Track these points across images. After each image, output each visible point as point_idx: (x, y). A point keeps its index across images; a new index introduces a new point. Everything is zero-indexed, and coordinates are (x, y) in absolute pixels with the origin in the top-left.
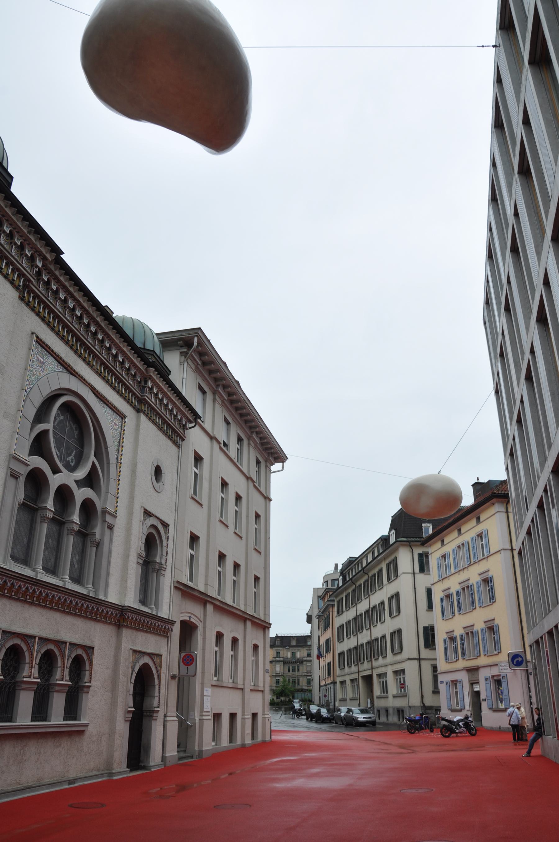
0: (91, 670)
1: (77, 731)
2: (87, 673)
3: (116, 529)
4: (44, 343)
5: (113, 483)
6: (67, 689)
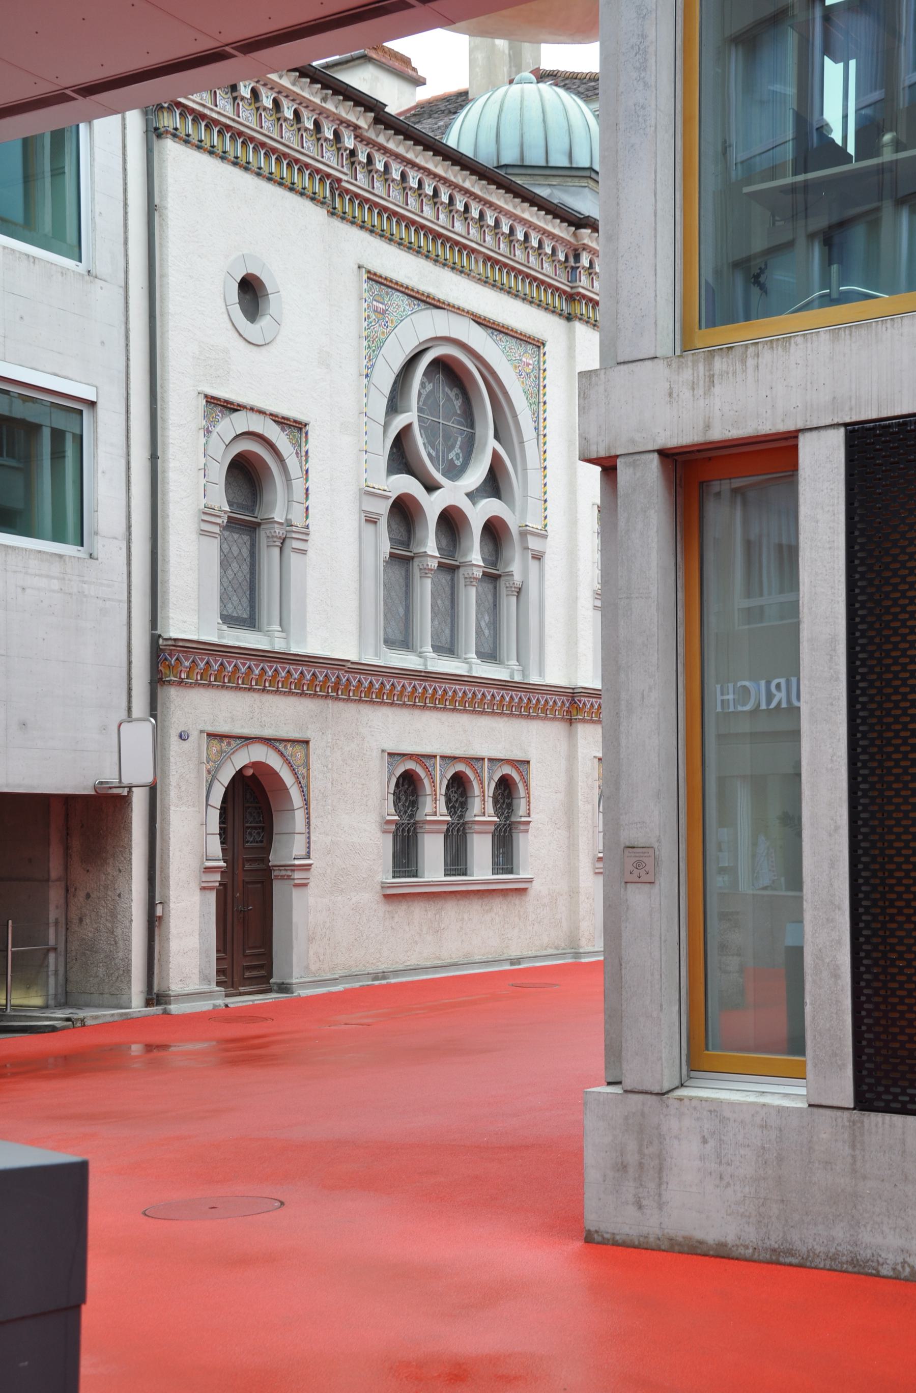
0: (529, 797)
1: (516, 889)
2: (523, 802)
3: (548, 560)
5: (534, 476)
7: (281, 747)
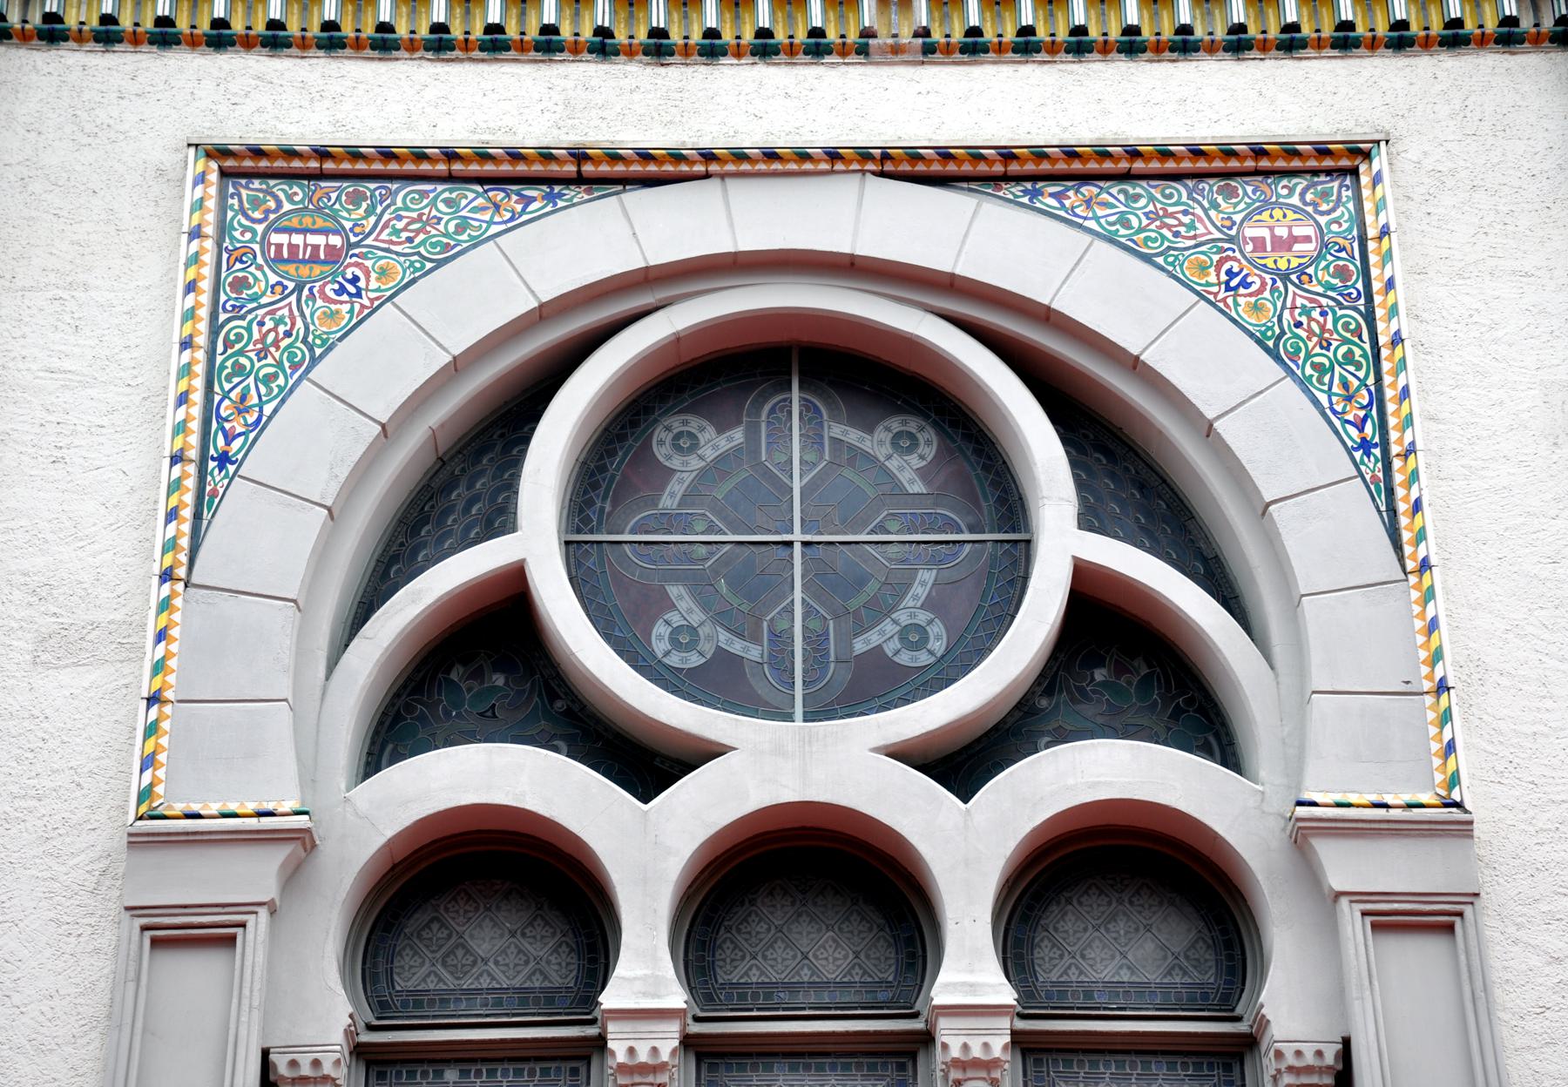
4: (354, 154)
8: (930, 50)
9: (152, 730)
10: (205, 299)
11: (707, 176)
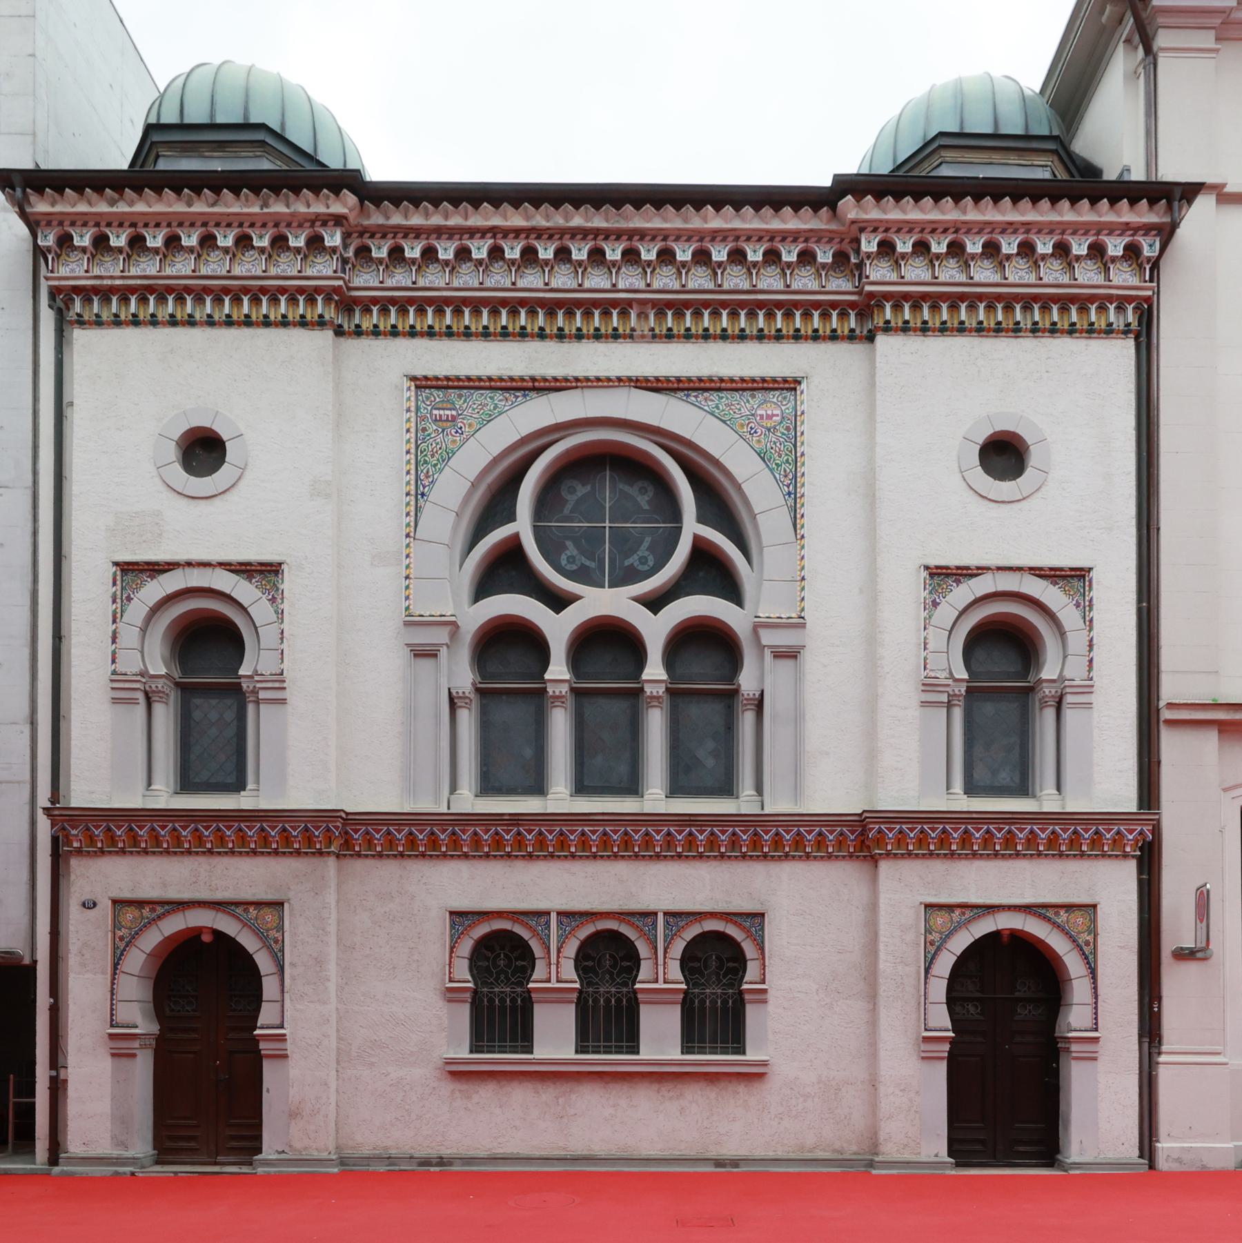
0: (764, 958)
4: (458, 379)
6: (575, 996)
7: (1050, 914)
8: (655, 337)
9: (407, 587)
10: (413, 435)
11: (577, 387)
